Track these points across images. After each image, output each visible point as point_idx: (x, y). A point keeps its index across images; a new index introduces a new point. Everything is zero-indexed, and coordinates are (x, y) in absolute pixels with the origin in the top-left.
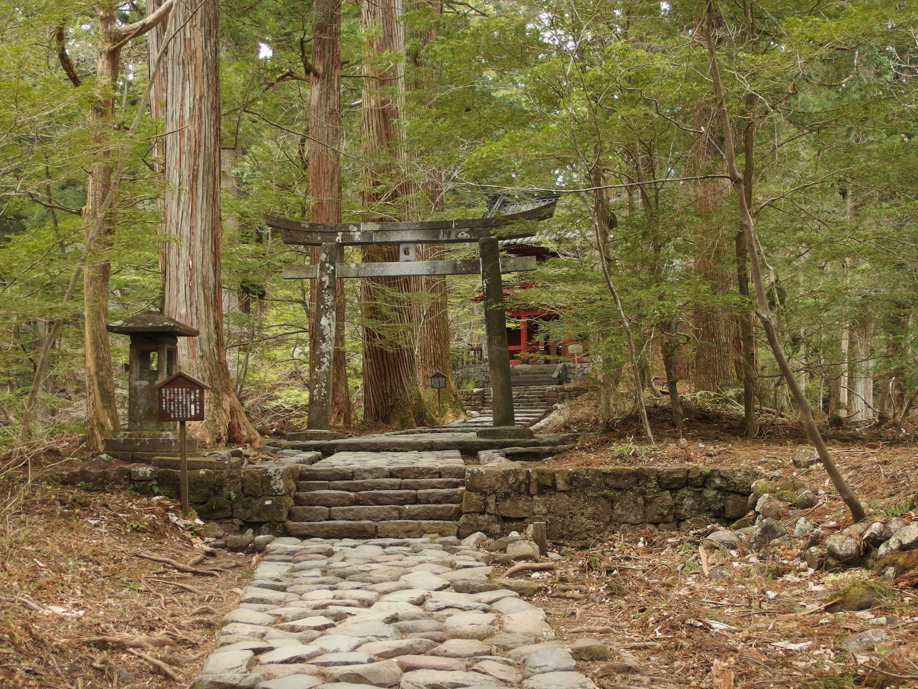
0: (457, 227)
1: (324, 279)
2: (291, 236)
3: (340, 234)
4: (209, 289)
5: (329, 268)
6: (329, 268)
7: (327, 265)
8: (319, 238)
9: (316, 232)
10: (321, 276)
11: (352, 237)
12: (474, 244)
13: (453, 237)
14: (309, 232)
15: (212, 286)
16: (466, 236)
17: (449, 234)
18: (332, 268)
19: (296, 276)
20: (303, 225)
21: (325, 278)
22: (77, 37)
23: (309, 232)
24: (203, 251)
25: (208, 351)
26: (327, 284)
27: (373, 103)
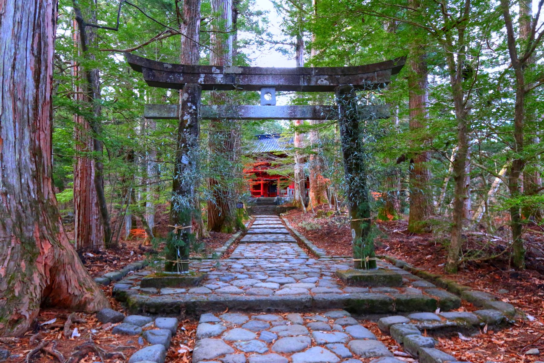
0: (317, 74)
1: (185, 118)
2: (154, 76)
3: (202, 76)
4: (24, 102)
5: (191, 108)
6: (191, 108)
7: (189, 104)
8: (182, 79)
9: (179, 73)
10: (183, 115)
11: (214, 79)
12: (329, 95)
13: (313, 83)
14: (172, 72)
15: (31, 99)
16: (325, 82)
17: (309, 81)
18: (194, 107)
19: (157, 115)
20: (165, 65)
21: (187, 117)
22: (168, 210)
23: (172, 72)
24: (17, 48)
25: (17, 187)
26: (189, 122)
27: (216, 62)
